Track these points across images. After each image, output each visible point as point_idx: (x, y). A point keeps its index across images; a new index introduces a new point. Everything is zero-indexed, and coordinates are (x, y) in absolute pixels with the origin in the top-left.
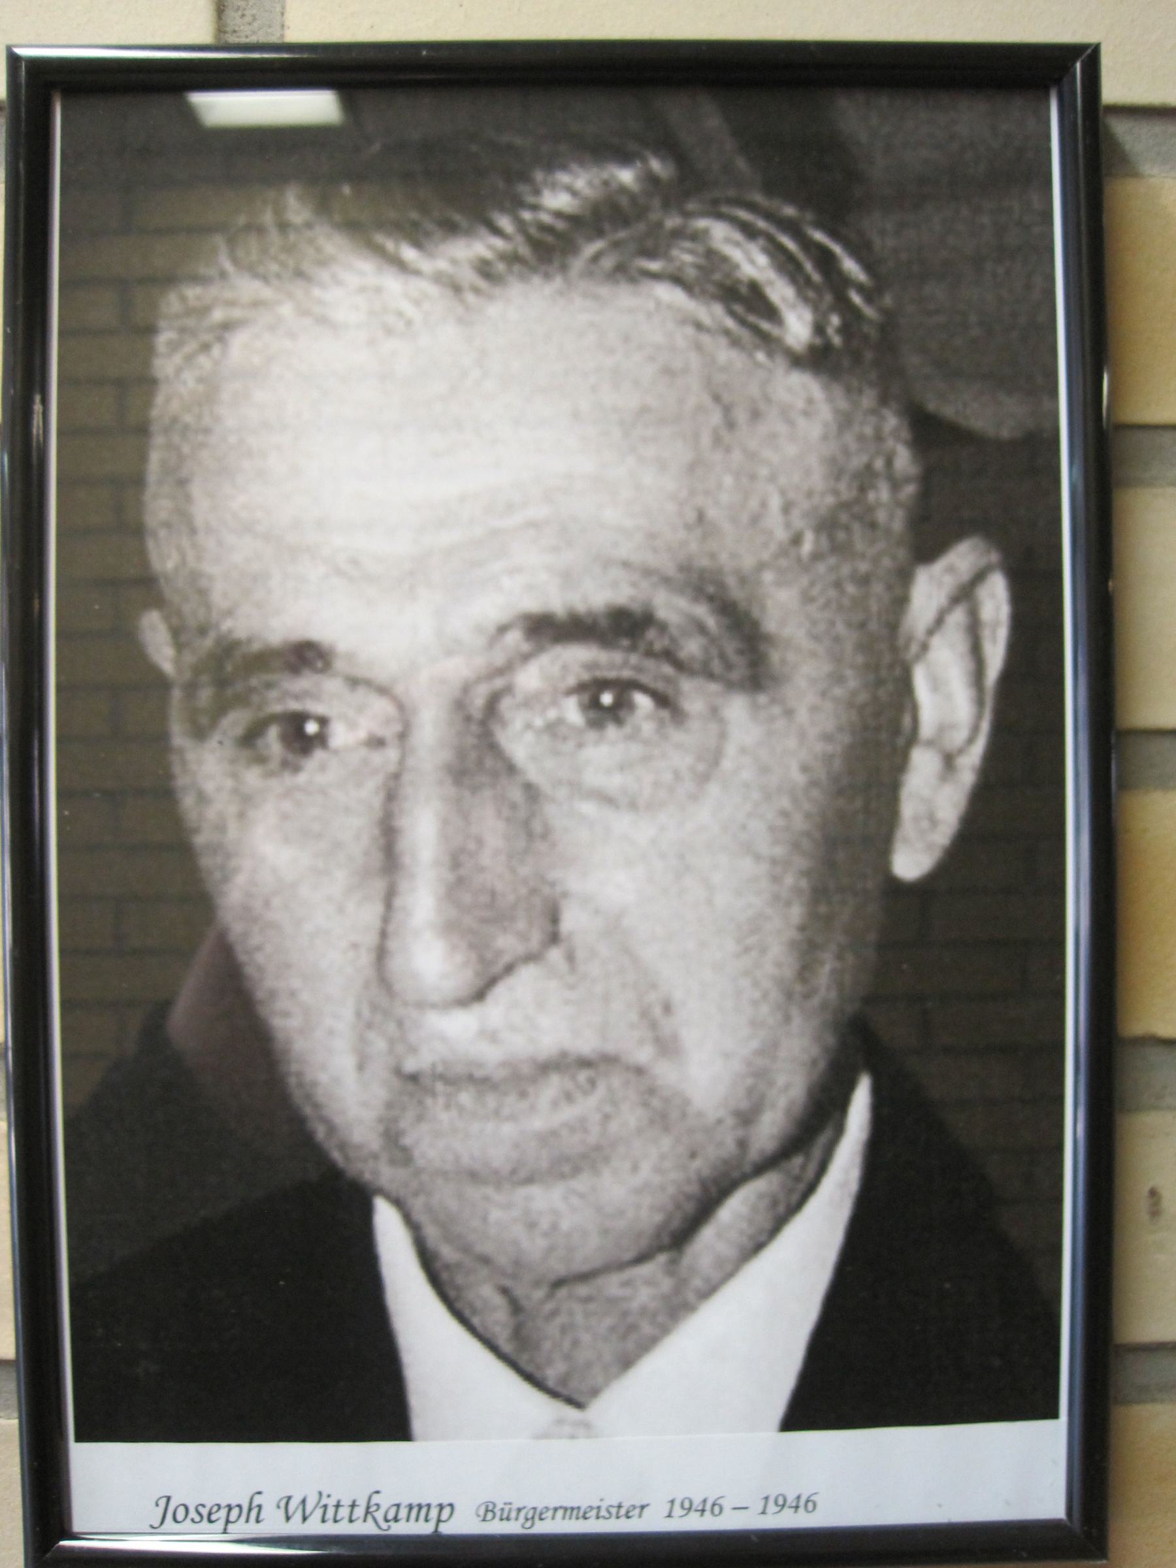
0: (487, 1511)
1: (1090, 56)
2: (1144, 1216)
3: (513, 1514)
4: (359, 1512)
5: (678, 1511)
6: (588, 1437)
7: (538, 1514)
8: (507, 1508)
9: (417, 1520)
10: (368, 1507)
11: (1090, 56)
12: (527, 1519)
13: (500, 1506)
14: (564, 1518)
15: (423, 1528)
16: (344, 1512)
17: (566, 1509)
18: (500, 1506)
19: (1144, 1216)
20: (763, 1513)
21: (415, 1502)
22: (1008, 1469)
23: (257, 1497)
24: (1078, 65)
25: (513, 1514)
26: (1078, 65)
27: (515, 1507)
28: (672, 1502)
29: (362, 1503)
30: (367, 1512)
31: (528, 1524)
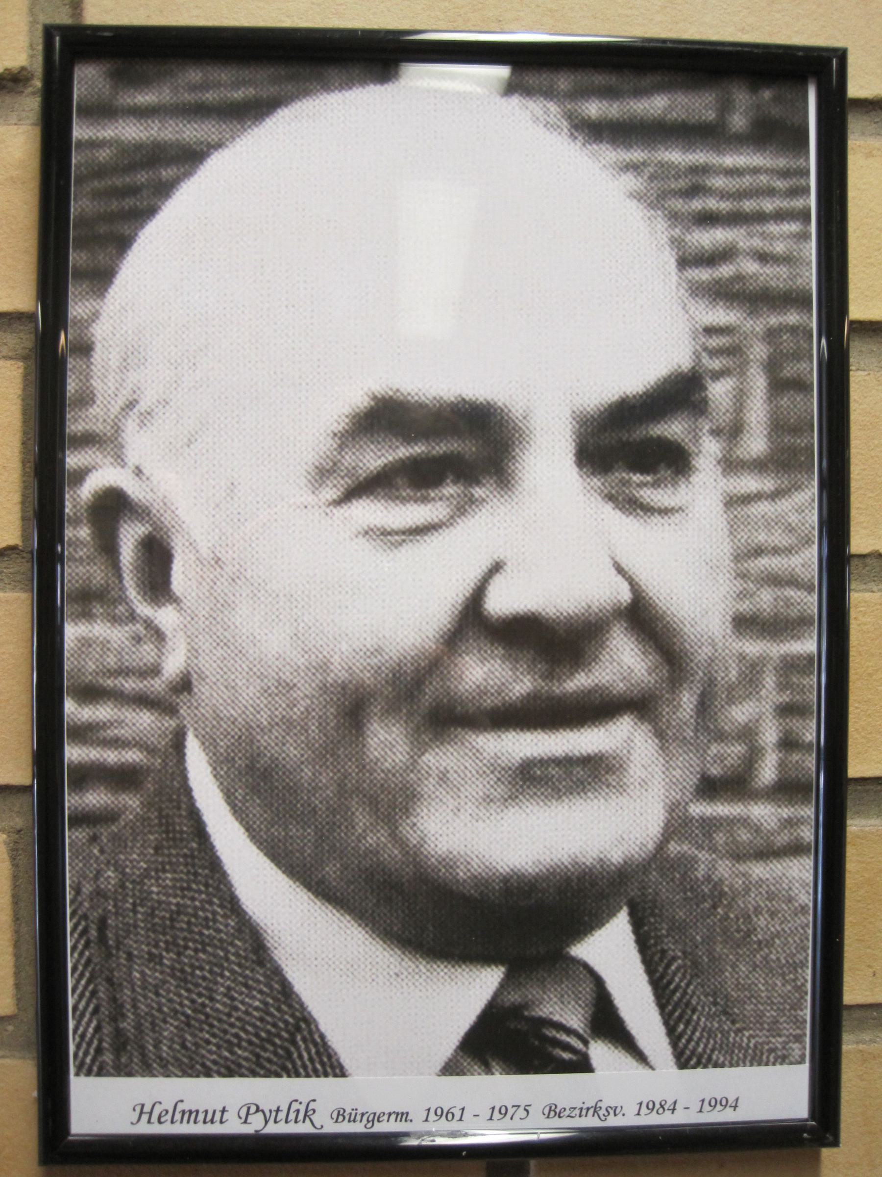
0: (338, 1114)
1: (835, 1143)
2: (593, 109)
3: (358, 1118)
4: (282, 1116)
5: (644, 1110)
6: (487, 1074)
7: (377, 1118)
8: (354, 1113)
9: (188, 1122)
10: (306, 1111)
11: (835, 1143)
12: (368, 1121)
13: (348, 1111)
14: (149, 1122)
15: (358, 1128)
16: (282, 1116)
17: (398, 1114)
18: (348, 1111)
19: (593, 109)
20: (426, 1120)
21: (400, 1111)
22: (776, 1092)
23: (179, 1104)
24: (57, 39)
25: (358, 1118)
26: (57, 39)
27: (359, 1112)
28: (703, 1101)
29: (284, 1108)
30: (305, 1115)
31: (370, 1125)
